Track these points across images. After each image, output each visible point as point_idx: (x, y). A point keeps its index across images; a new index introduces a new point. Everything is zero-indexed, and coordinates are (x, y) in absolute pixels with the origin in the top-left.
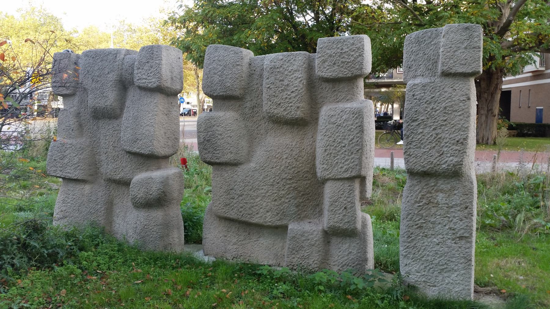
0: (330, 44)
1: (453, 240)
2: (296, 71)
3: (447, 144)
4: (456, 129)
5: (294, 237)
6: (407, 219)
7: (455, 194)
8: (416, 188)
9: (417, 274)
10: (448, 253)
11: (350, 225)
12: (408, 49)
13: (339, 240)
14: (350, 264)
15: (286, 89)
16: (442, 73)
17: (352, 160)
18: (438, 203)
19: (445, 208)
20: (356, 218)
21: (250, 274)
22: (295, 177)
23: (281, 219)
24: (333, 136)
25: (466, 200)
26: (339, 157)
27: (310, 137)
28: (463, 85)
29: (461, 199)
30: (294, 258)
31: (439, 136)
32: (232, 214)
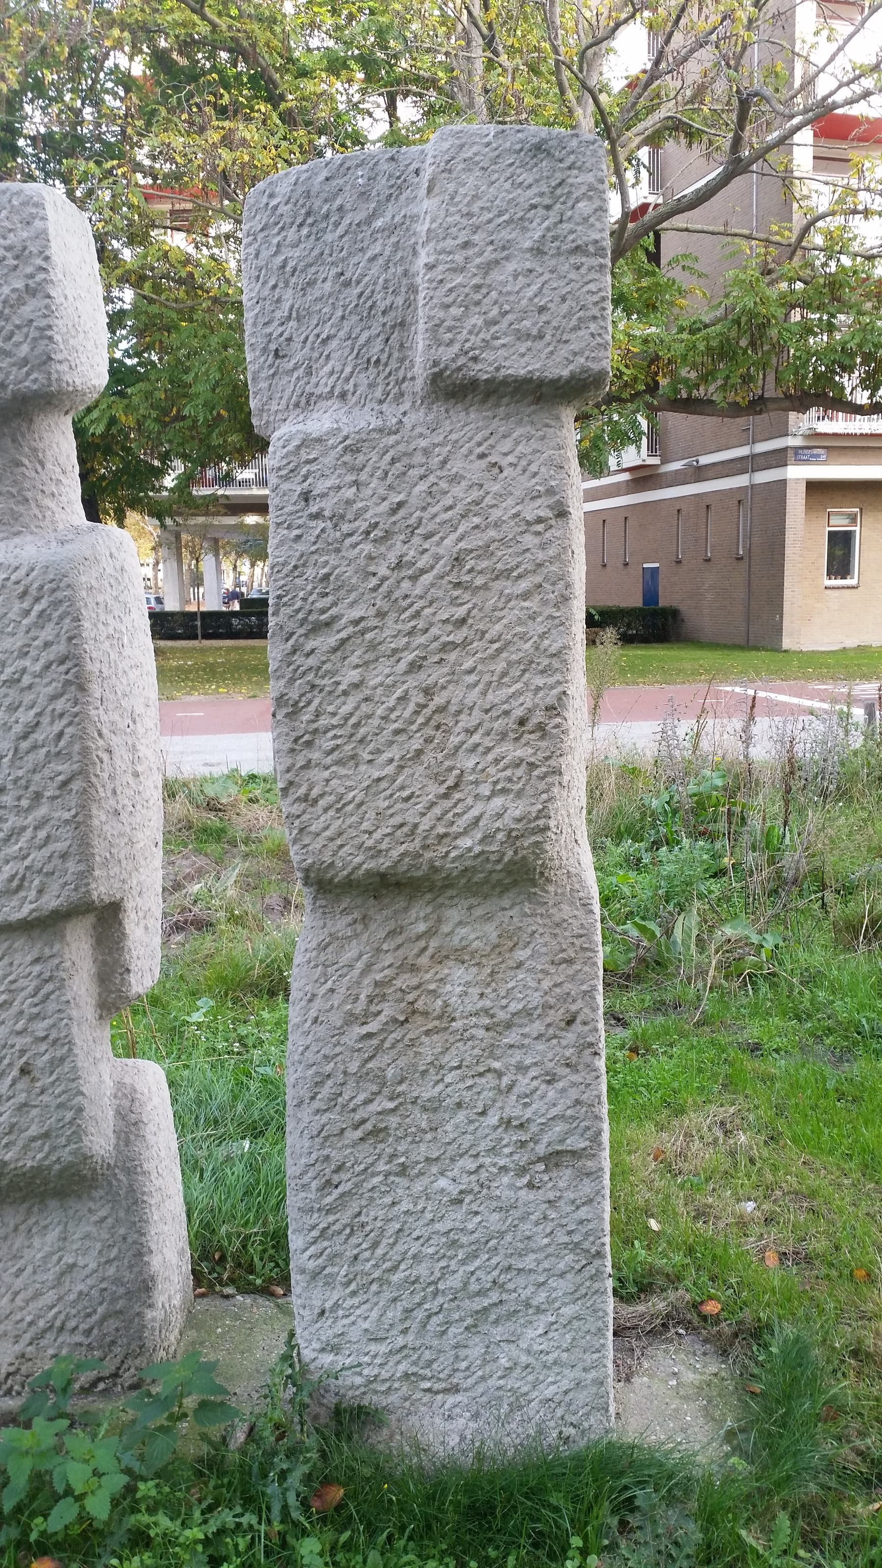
1: (522, 1171)
3: (476, 738)
4: (510, 664)
6: (316, 1104)
7: (520, 965)
8: (349, 955)
9: (373, 1348)
10: (502, 1234)
11: (54, 1149)
12: (265, 254)
14: (72, 1323)
16: (436, 379)
17: (42, 834)
18: (447, 1015)
19: (481, 1033)
20: (80, 1110)
25: (567, 987)
28: (534, 444)
29: (546, 984)
31: (439, 700)
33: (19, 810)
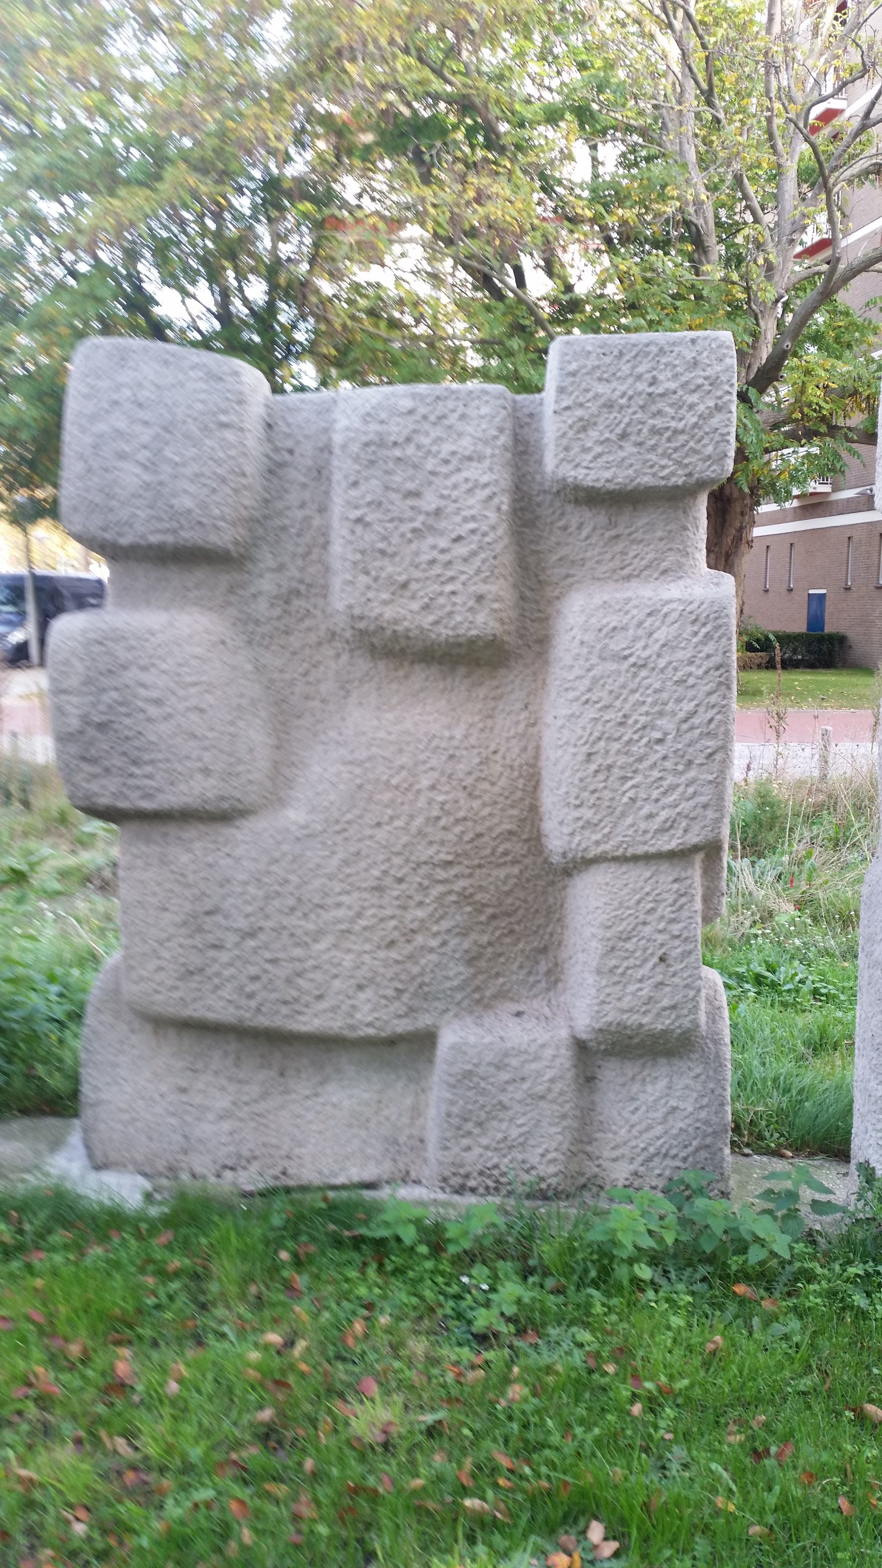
0: (608, 360)
2: (470, 459)
5: (468, 1075)
11: (678, 1017)
13: (630, 1069)
14: (673, 1152)
15: (431, 528)
17: (691, 790)
21: (338, 1243)
22: (466, 854)
23: (412, 1010)
24: (618, 703)
26: (638, 779)
27: (519, 705)
30: (468, 1149)
32: (217, 1007)
33: (676, 773)
